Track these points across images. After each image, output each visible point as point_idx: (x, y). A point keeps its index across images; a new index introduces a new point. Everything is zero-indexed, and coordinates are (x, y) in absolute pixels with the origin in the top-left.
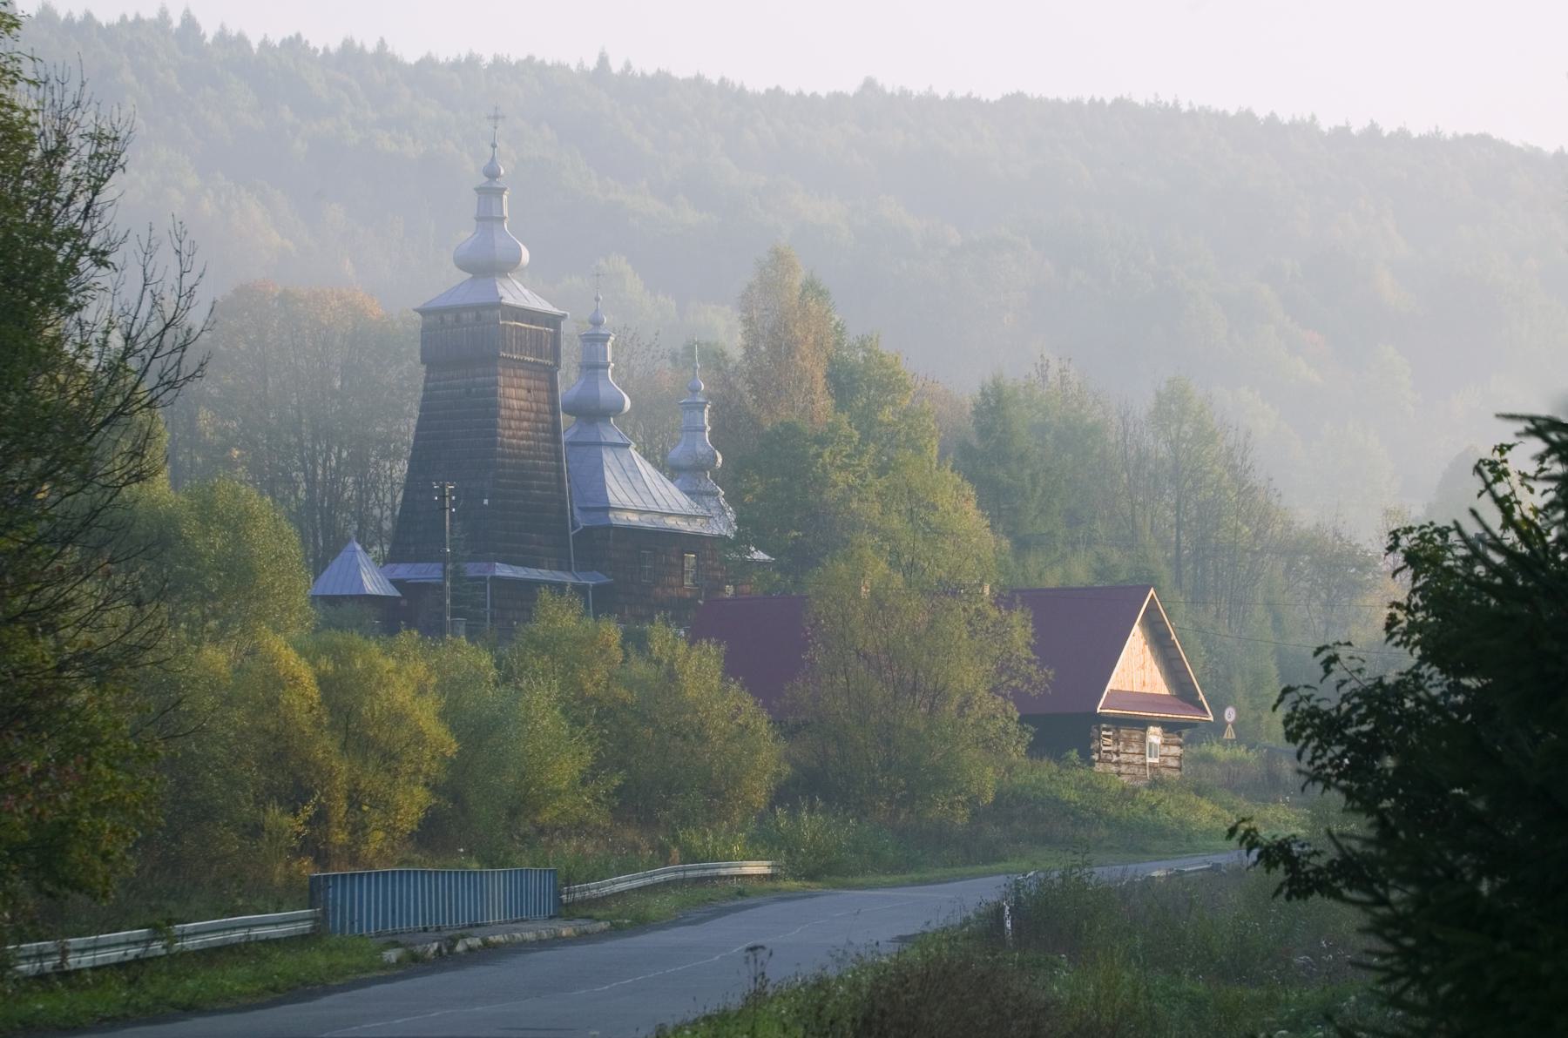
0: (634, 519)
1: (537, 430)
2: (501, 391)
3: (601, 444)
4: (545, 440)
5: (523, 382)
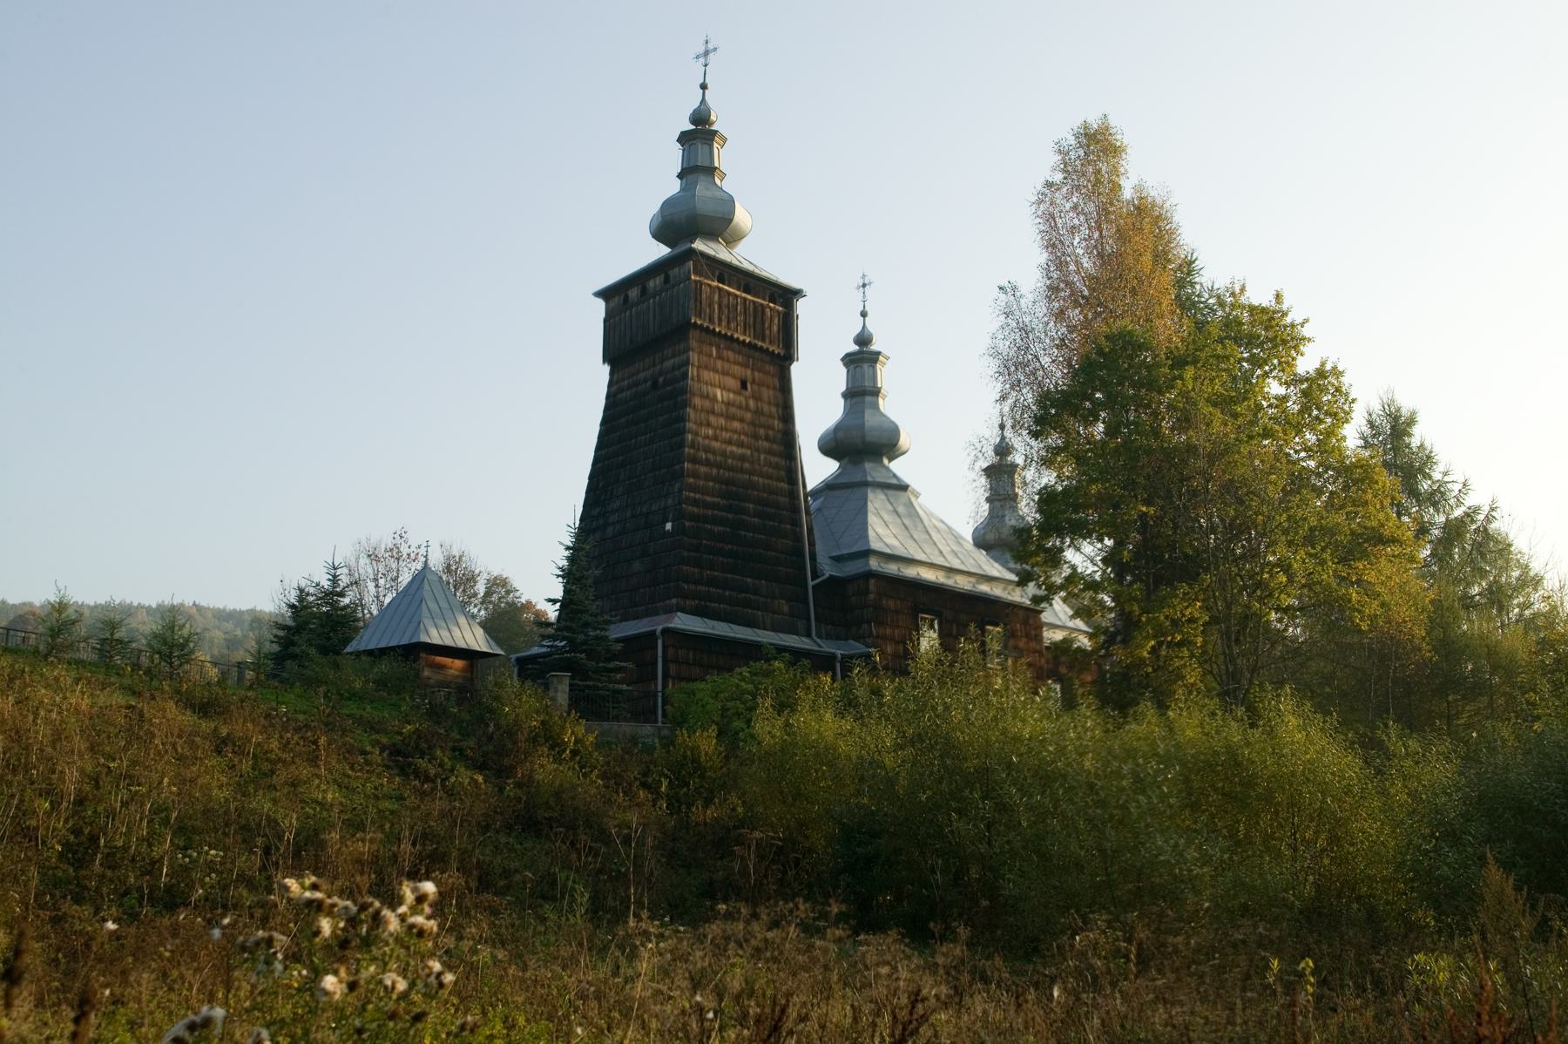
0: (929, 575)
1: (756, 437)
2: (692, 371)
3: (866, 484)
4: (770, 452)
5: (737, 369)
